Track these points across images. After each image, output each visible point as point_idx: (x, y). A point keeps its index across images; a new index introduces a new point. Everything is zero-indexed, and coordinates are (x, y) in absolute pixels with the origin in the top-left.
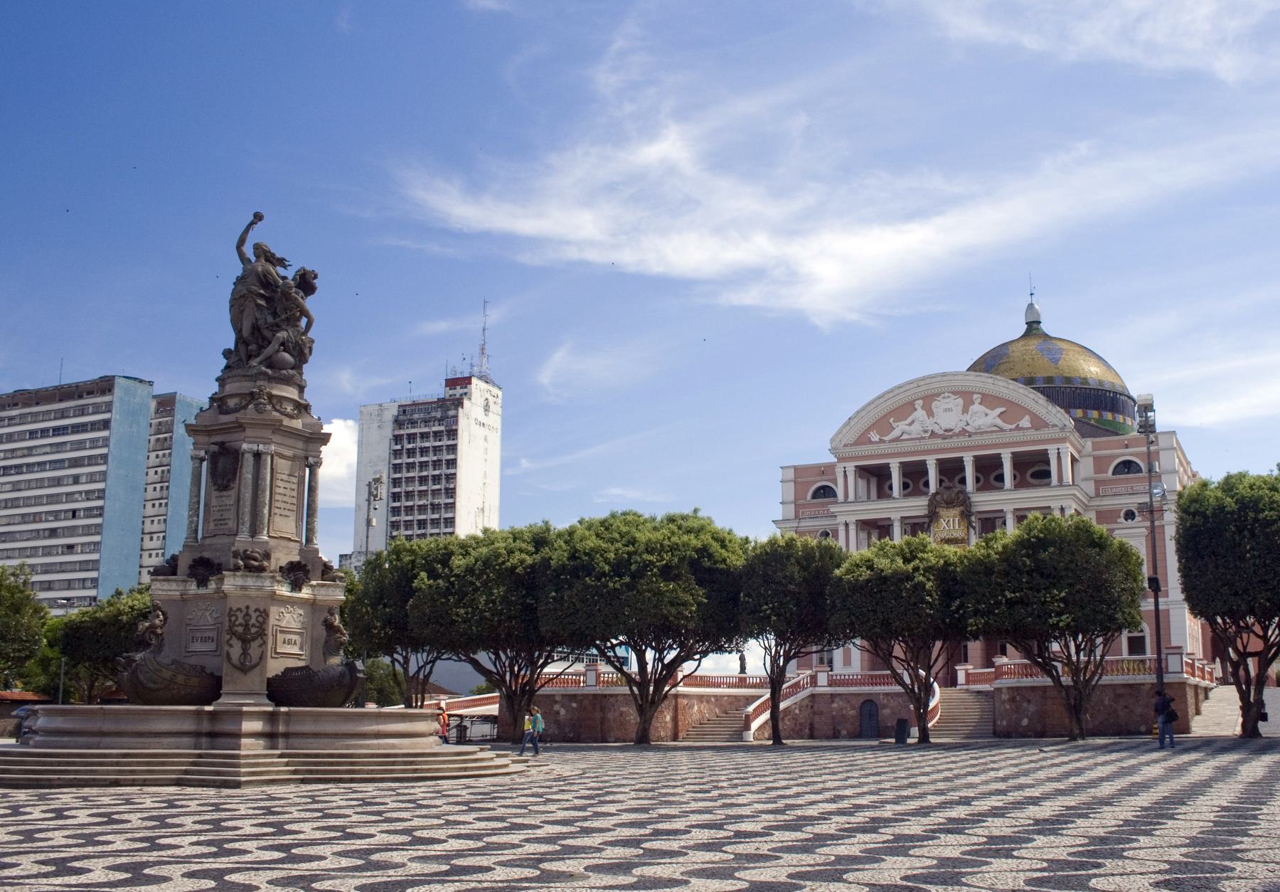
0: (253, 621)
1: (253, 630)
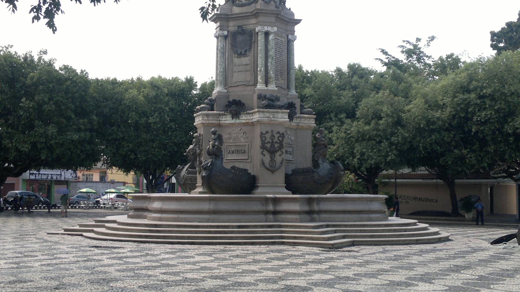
0: (276, 140)
1: (276, 145)
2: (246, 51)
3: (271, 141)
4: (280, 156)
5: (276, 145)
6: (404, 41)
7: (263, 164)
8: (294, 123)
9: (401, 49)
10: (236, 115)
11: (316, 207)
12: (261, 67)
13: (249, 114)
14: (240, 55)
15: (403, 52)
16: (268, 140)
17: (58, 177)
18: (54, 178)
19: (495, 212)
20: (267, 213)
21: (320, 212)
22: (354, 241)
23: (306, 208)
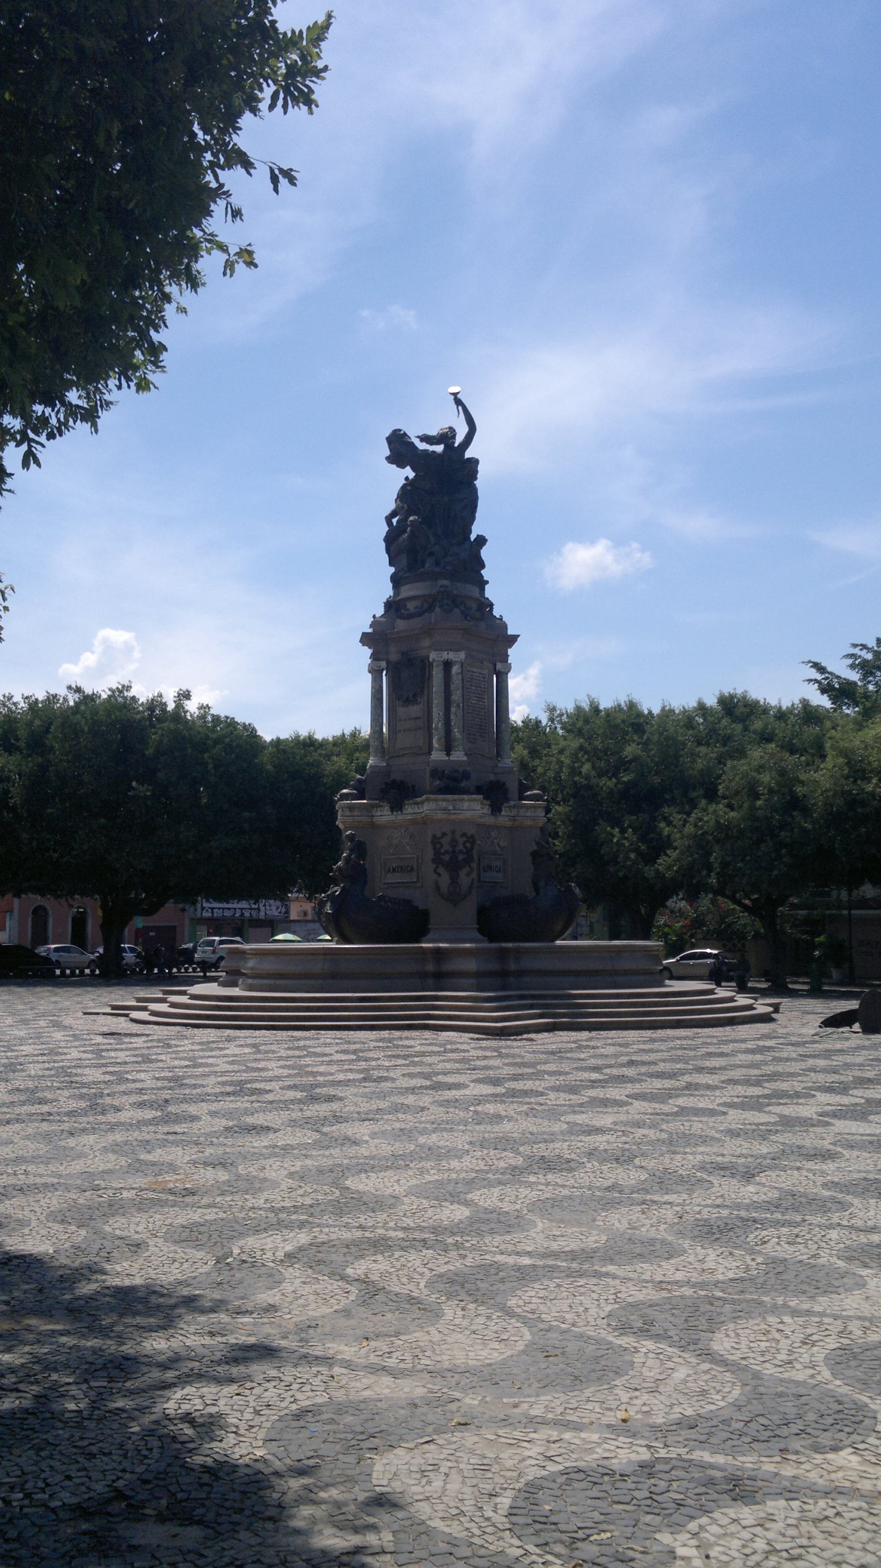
1: (461, 857)
2: (415, 695)
3: (450, 850)
4: (468, 875)
5: (461, 857)
6: (855, 646)
7: (438, 888)
8: (504, 818)
9: (850, 661)
10: (397, 806)
11: (449, 967)
12: (437, 723)
13: (417, 804)
14: (407, 702)
15: (852, 667)
16: (447, 847)
17: (254, 913)
18: (247, 914)
20: (423, 975)
21: (521, 973)
22: (555, 1023)
23: (494, 966)
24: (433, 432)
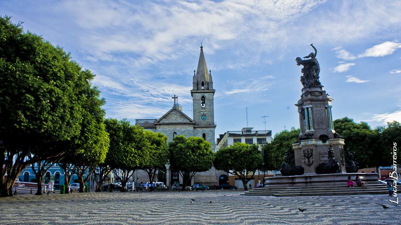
0: (310, 152)
19: (193, 94)
24: (308, 55)
